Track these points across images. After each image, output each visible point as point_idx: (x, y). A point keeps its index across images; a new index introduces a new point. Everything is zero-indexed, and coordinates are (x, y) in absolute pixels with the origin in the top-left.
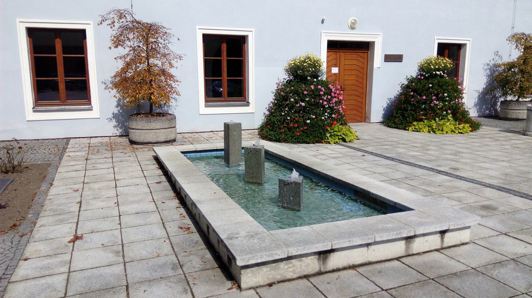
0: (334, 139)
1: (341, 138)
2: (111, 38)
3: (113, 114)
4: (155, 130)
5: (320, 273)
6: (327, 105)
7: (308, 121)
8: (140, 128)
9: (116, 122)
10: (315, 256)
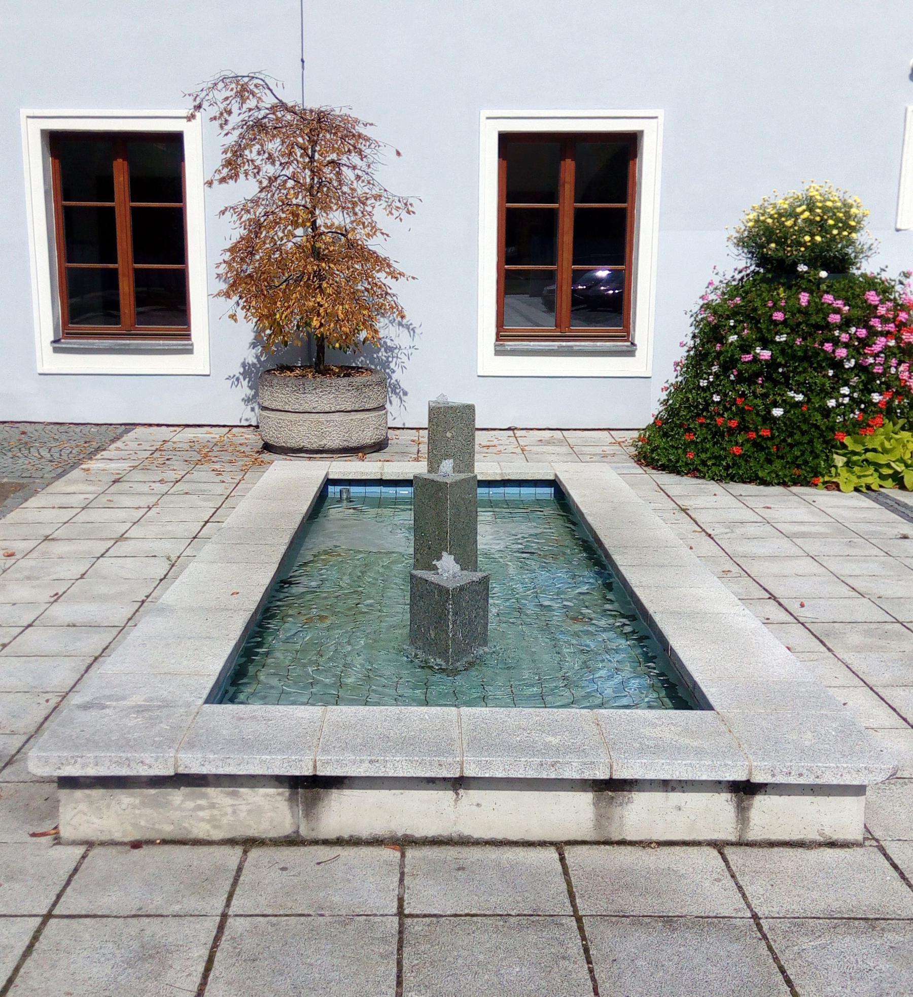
0: (859, 477)
1: (889, 476)
2: (224, 156)
3: (244, 365)
4: (317, 415)
5: (293, 841)
6: (849, 360)
7: (778, 412)
8: (279, 408)
9: (251, 388)
10: (281, 790)
